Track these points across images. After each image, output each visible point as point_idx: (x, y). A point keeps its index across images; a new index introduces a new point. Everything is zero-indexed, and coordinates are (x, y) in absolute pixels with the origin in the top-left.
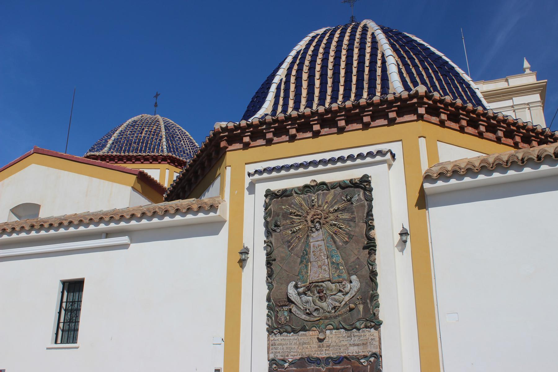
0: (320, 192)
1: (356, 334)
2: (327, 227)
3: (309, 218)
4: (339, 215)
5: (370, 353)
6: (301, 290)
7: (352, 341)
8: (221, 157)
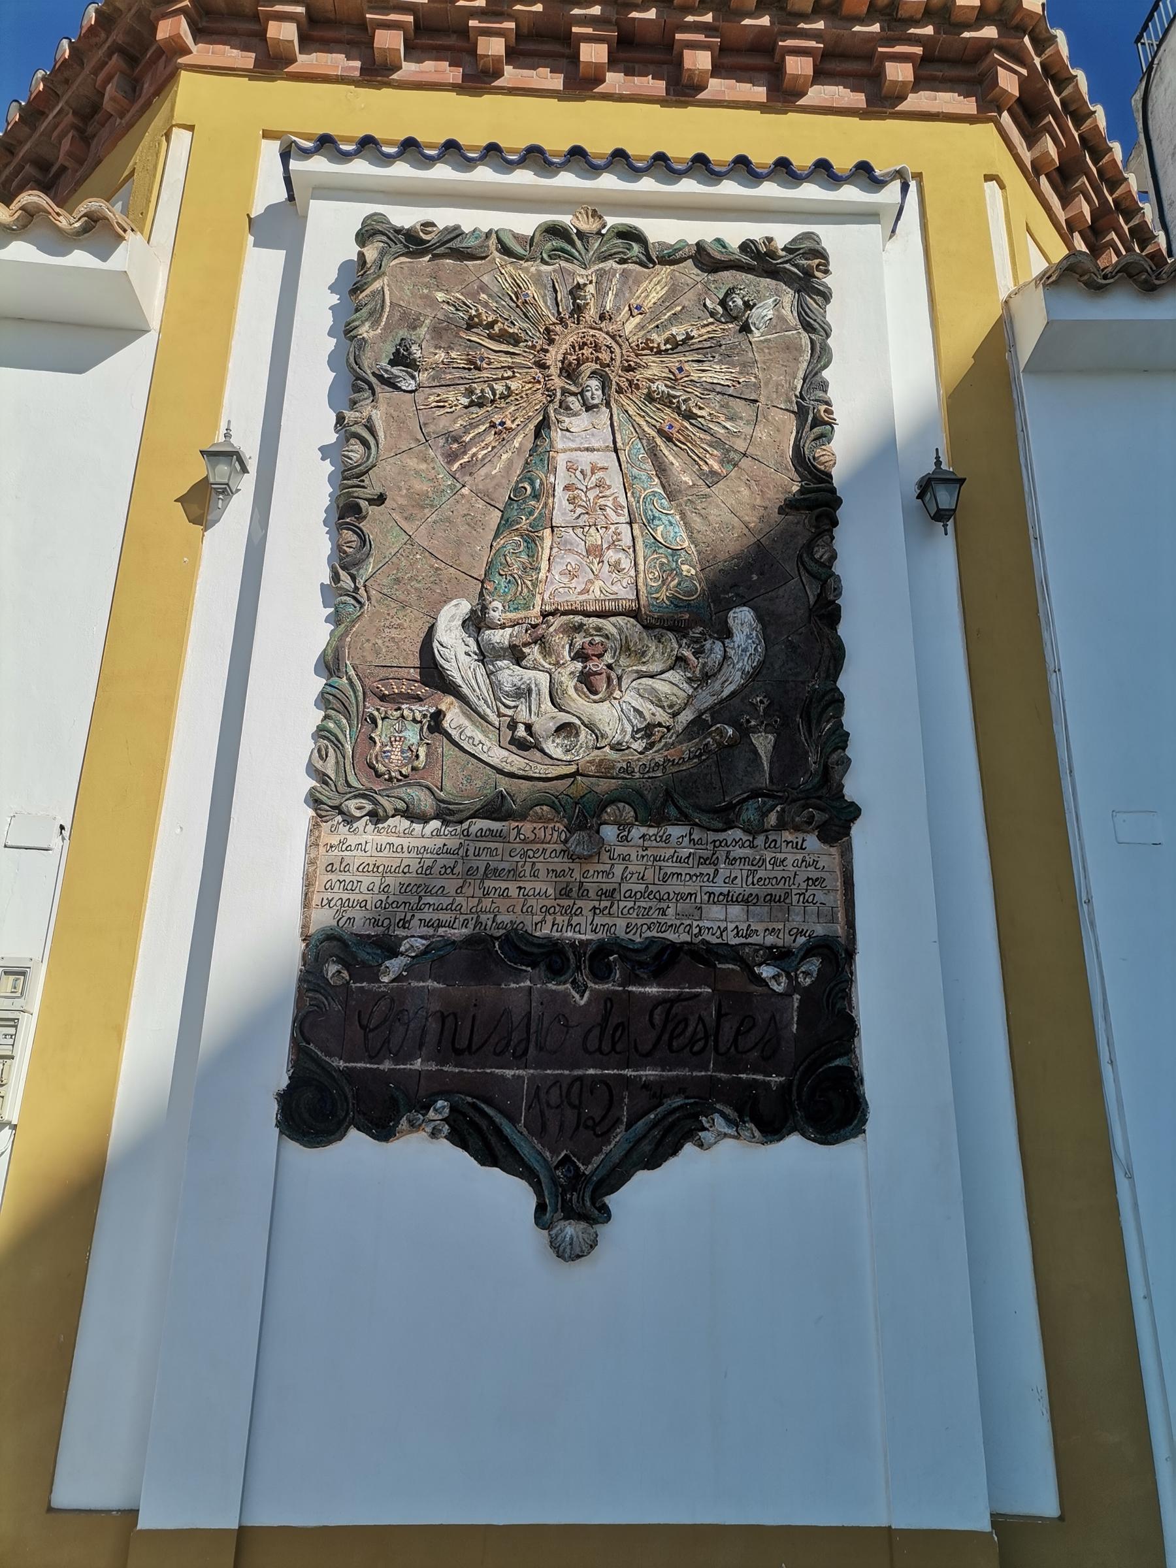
0: (611, 264)
1: (738, 852)
2: (630, 404)
3: (554, 357)
4: (686, 367)
5: (802, 940)
6: (500, 637)
7: (719, 880)
8: (130, 126)
